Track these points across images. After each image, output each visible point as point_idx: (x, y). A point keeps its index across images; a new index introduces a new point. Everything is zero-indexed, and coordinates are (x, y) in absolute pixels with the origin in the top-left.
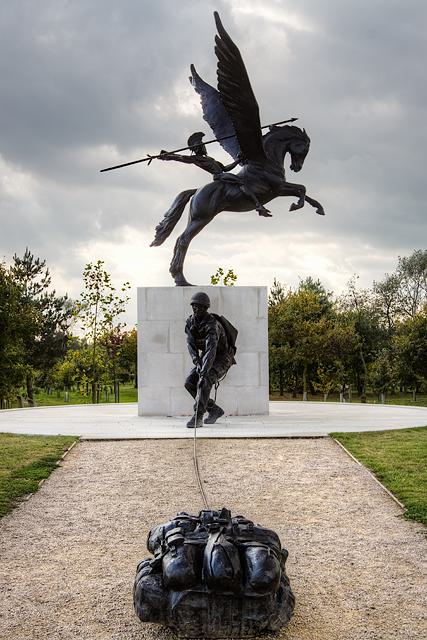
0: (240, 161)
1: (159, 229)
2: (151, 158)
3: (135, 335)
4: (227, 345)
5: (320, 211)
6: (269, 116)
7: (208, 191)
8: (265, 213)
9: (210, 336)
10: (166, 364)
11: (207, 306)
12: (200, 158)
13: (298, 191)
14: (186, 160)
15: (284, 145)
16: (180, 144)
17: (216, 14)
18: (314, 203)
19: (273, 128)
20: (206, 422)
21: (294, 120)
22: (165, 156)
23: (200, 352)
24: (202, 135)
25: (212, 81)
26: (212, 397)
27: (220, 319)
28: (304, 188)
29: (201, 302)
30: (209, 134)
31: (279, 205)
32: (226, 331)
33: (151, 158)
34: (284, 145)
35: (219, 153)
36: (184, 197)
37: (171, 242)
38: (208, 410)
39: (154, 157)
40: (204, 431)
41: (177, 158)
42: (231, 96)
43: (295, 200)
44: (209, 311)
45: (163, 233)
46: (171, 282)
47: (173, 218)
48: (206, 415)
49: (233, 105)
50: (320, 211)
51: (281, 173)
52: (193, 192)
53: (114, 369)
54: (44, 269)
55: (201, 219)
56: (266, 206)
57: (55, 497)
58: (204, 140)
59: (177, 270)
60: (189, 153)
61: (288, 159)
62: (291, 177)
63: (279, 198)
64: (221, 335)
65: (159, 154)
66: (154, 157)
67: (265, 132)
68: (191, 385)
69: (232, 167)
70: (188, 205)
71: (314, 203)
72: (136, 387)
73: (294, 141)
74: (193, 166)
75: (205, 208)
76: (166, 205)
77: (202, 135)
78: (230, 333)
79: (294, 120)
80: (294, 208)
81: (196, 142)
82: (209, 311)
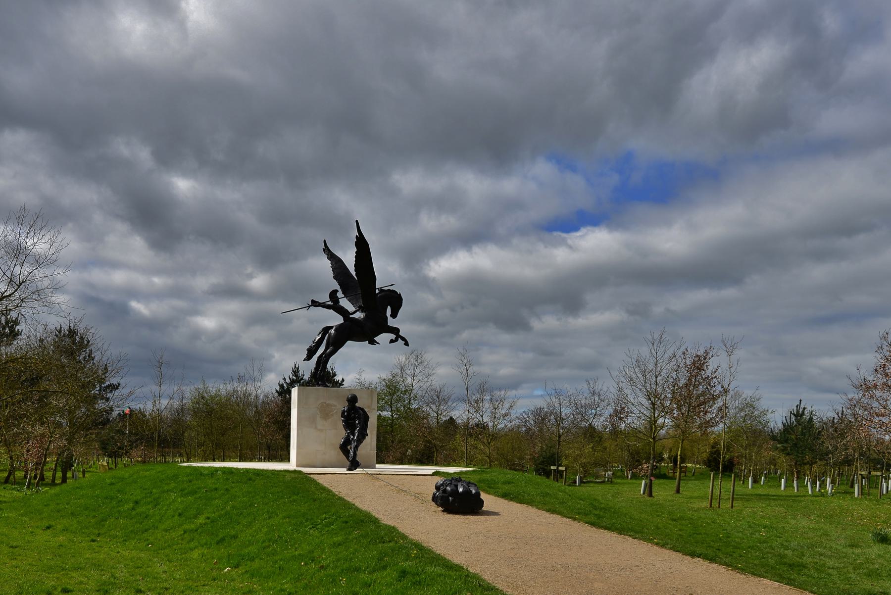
0: (361, 309)
5: (407, 344)
6: (381, 283)
7: (339, 328)
13: (396, 331)
14: (329, 307)
16: (325, 298)
18: (403, 339)
19: (381, 290)
22: (315, 304)
24: (337, 291)
27: (363, 409)
30: (340, 294)
31: (384, 338)
35: (345, 303)
36: (326, 330)
37: (315, 358)
43: (393, 336)
44: (357, 405)
45: (311, 353)
47: (318, 344)
50: (407, 344)
52: (331, 327)
61: (389, 309)
62: (391, 322)
67: (377, 291)
69: (355, 312)
73: (394, 300)
77: (337, 291)
80: (392, 341)
81: (333, 295)
82: (357, 405)
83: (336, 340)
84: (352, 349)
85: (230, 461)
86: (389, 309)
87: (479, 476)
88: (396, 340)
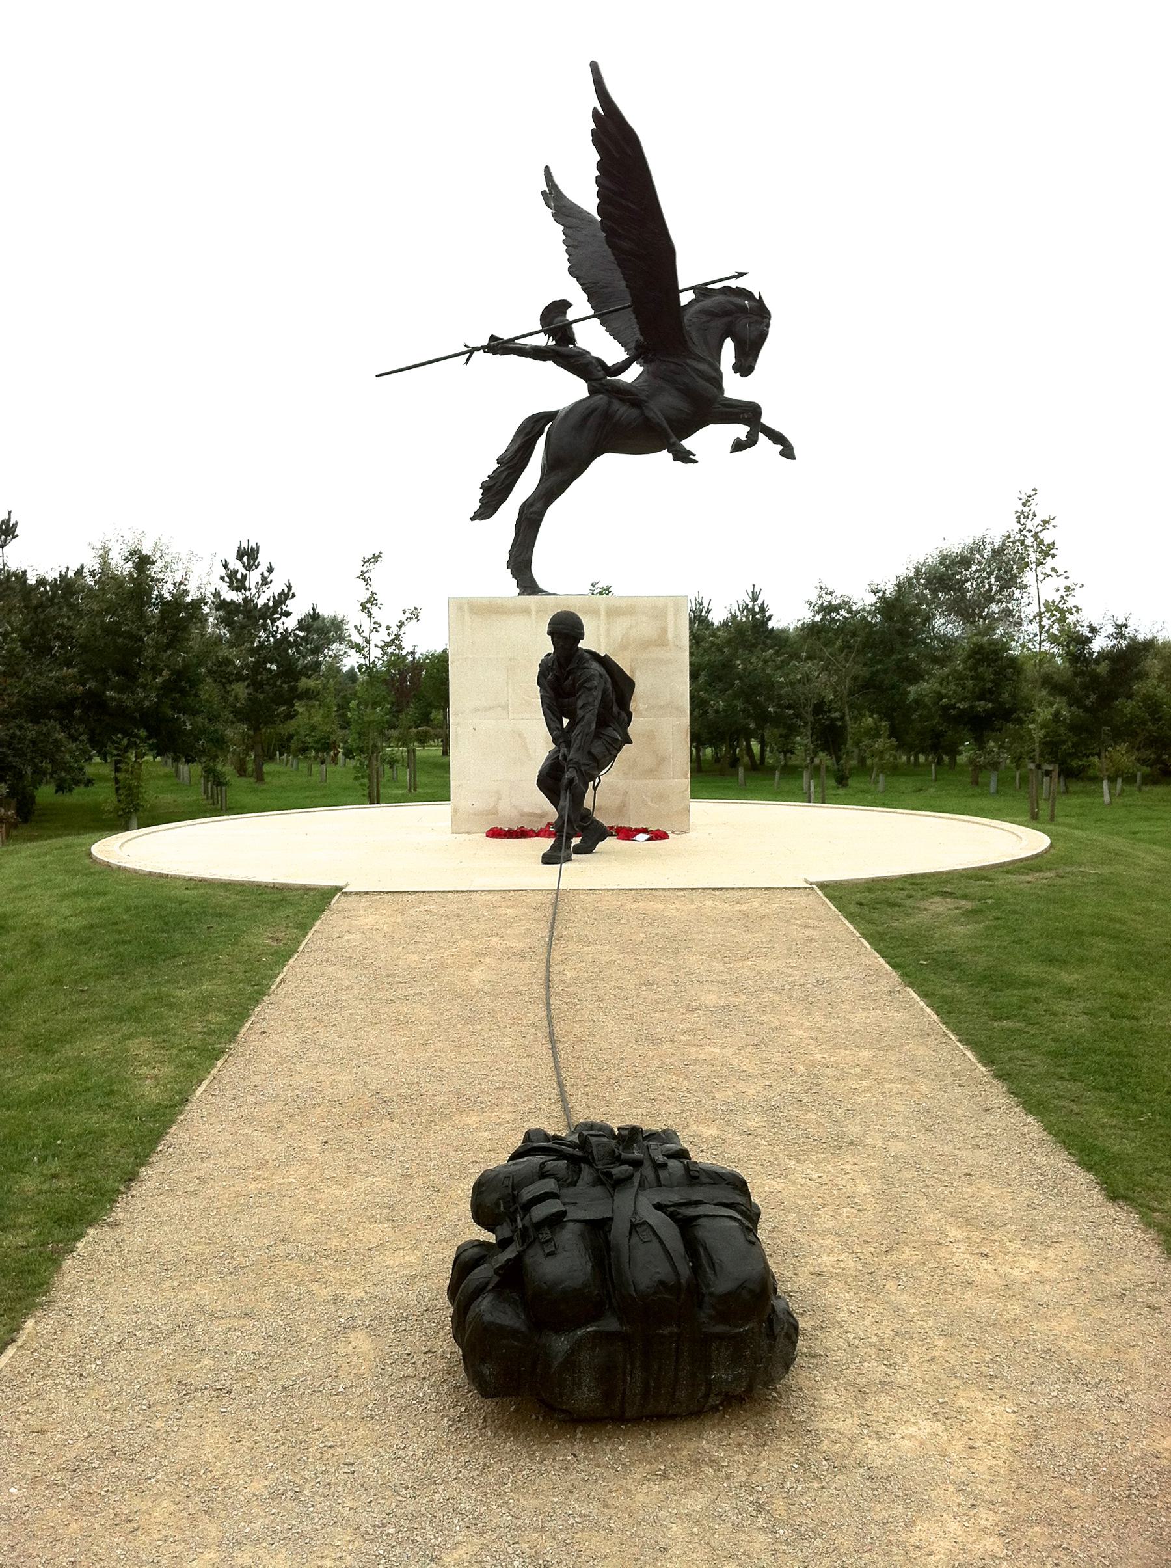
0: (637, 354)
1: (485, 487)
2: (471, 351)
3: (445, 651)
4: (615, 709)
5: (788, 452)
6: (694, 269)
7: (579, 414)
8: (684, 456)
9: (583, 695)
10: (499, 735)
12: (560, 347)
13: (749, 414)
14: (538, 354)
15: (719, 323)
16: (524, 322)
17: (595, 68)
18: (776, 437)
19: (702, 291)
20: (579, 850)
21: (740, 275)
22: (497, 346)
23: (566, 721)
25: (584, 194)
26: (588, 803)
27: (605, 662)
28: (759, 407)
29: (565, 630)
30: (580, 305)
32: (615, 683)
33: (471, 351)
34: (719, 323)
35: (596, 340)
36: (531, 429)
38: (575, 830)
39: (477, 349)
40: (582, 873)
41: (523, 352)
42: (622, 232)
43: (741, 431)
45: (494, 493)
46: (510, 586)
49: (626, 245)
50: (788, 452)
51: (716, 380)
53: (389, 725)
54: (86, 572)
55: (562, 472)
56: (688, 443)
57: (299, 982)
58: (571, 315)
59: (520, 562)
60: (541, 340)
61: (729, 350)
62: (735, 387)
63: (711, 427)
64: (605, 692)
65: (485, 342)
66: (477, 349)
67: (686, 298)
68: (552, 780)
69: (623, 367)
70: (541, 442)
72: (446, 753)
73: (741, 318)
74: (549, 367)
75: (564, 448)
76: (502, 441)
78: (619, 687)
79: (740, 275)
80: (738, 446)
81: (555, 316)
82: (582, 645)
83: (564, 448)
84: (615, 478)
85: (216, 802)
87: (117, 936)
88: (751, 441)
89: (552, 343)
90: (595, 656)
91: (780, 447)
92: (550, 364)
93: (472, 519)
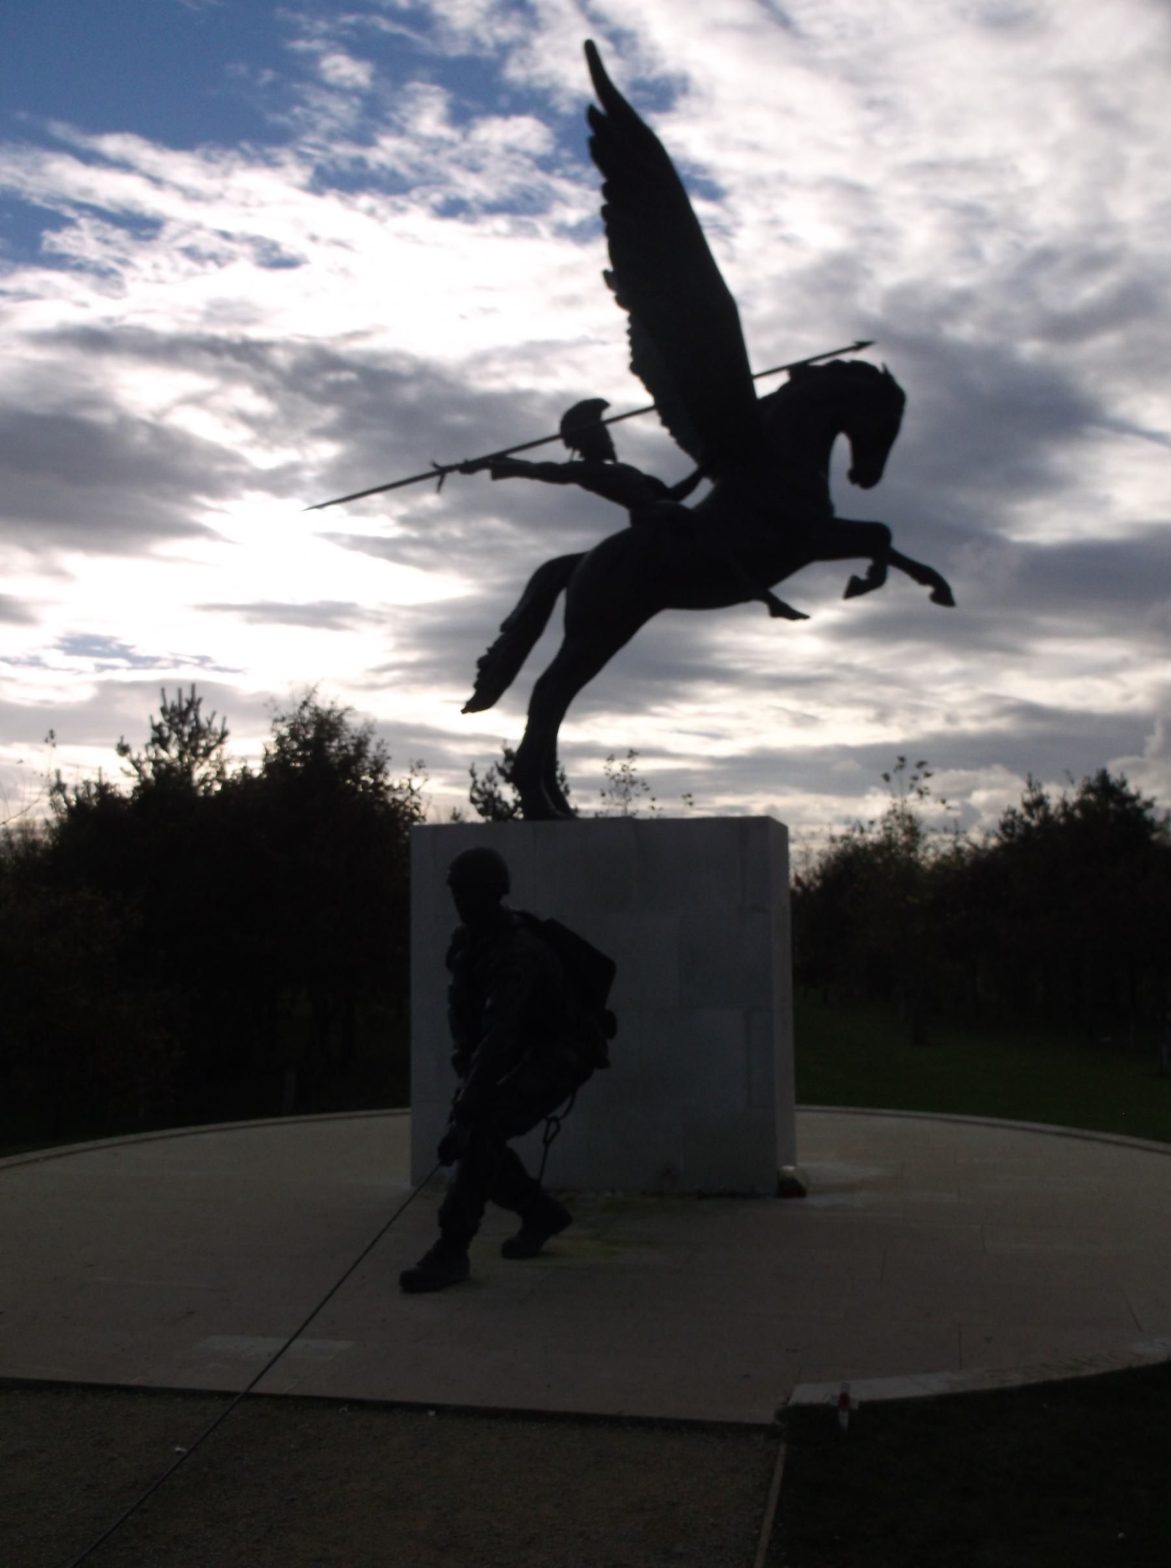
11: (503, 887)
43: (861, 567)
44: (512, 902)
48: (499, 1224)
58: (606, 415)
60: (560, 453)
62: (848, 501)
66: (450, 469)
69: (688, 485)
71: (923, 574)
86: (842, 445)
89: (577, 457)
90: (529, 920)
91: (928, 590)
92: (574, 489)
93: (464, 711)
